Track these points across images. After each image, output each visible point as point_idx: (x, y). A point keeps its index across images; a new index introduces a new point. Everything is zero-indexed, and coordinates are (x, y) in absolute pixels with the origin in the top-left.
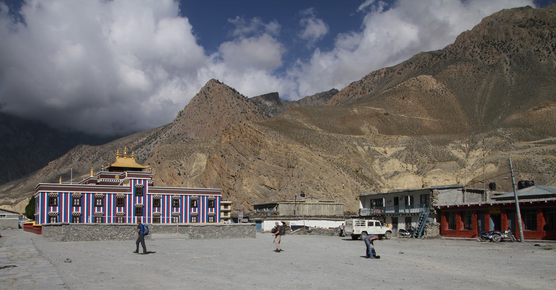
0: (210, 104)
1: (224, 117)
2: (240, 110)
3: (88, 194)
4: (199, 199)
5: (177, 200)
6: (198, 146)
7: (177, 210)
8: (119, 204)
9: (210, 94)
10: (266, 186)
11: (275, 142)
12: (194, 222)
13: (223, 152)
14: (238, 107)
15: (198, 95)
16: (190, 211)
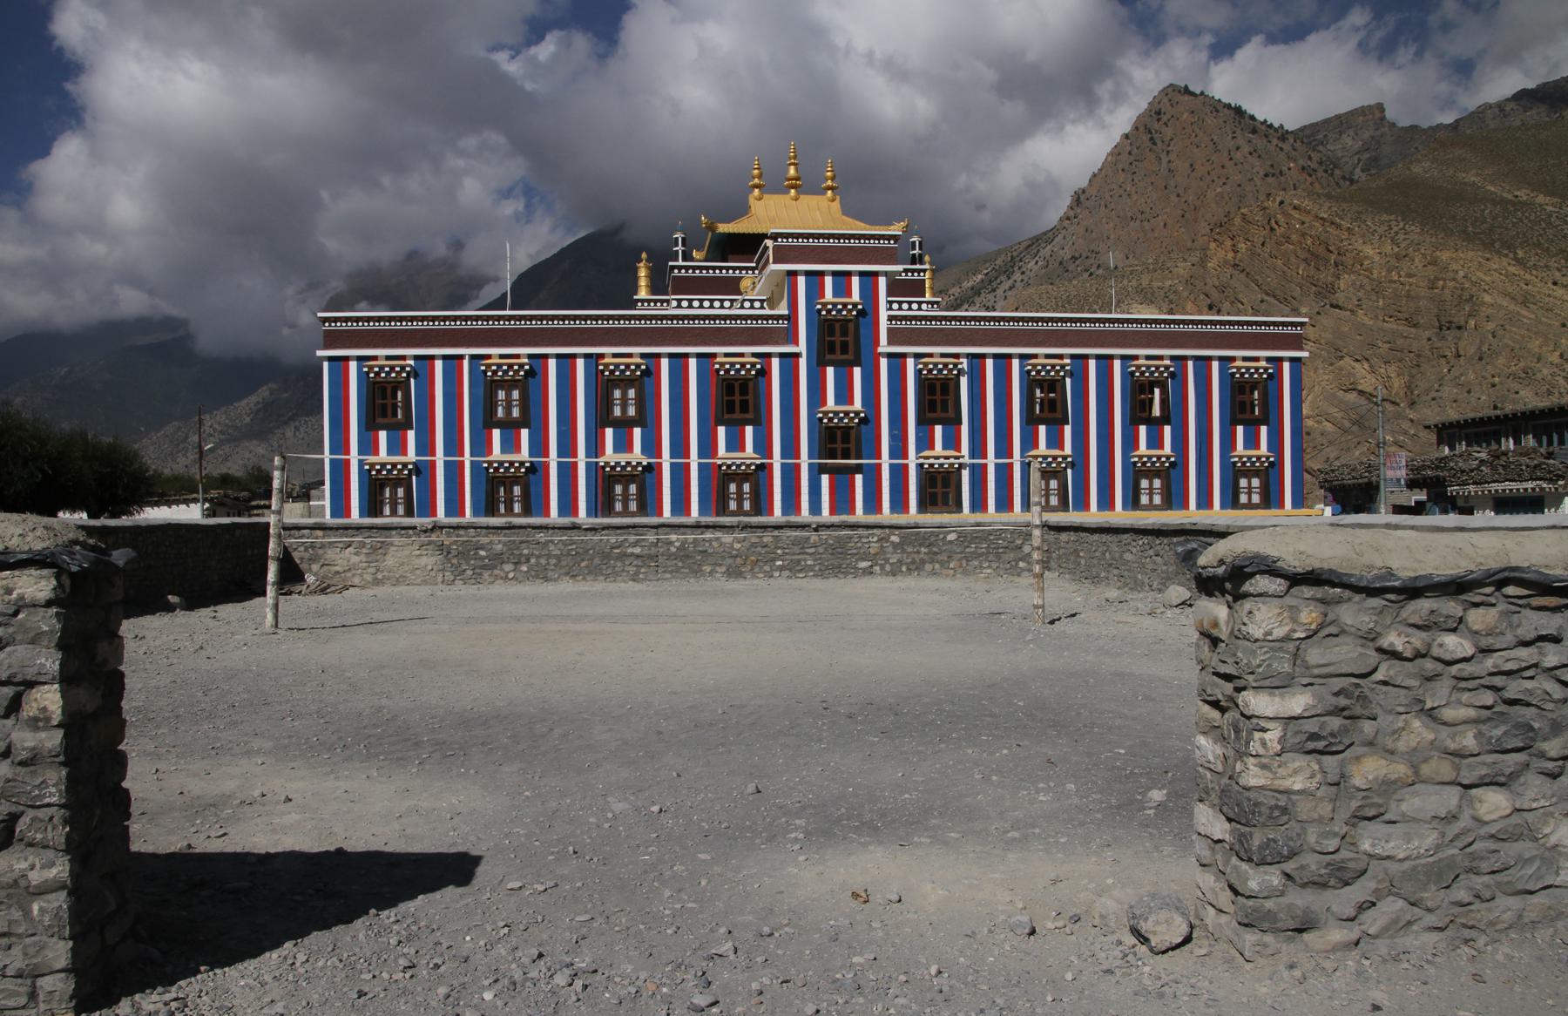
0: (1165, 159)
1: (1210, 194)
2: (1259, 167)
3: (566, 361)
4: (1179, 377)
5: (1053, 385)
6: (1134, 283)
7: (1056, 441)
8: (730, 408)
9: (1164, 129)
10: (1361, 393)
11: (1388, 248)
12: (1151, 507)
13: (1214, 294)
14: (1254, 160)
15: (1127, 136)
16: (1131, 442)
